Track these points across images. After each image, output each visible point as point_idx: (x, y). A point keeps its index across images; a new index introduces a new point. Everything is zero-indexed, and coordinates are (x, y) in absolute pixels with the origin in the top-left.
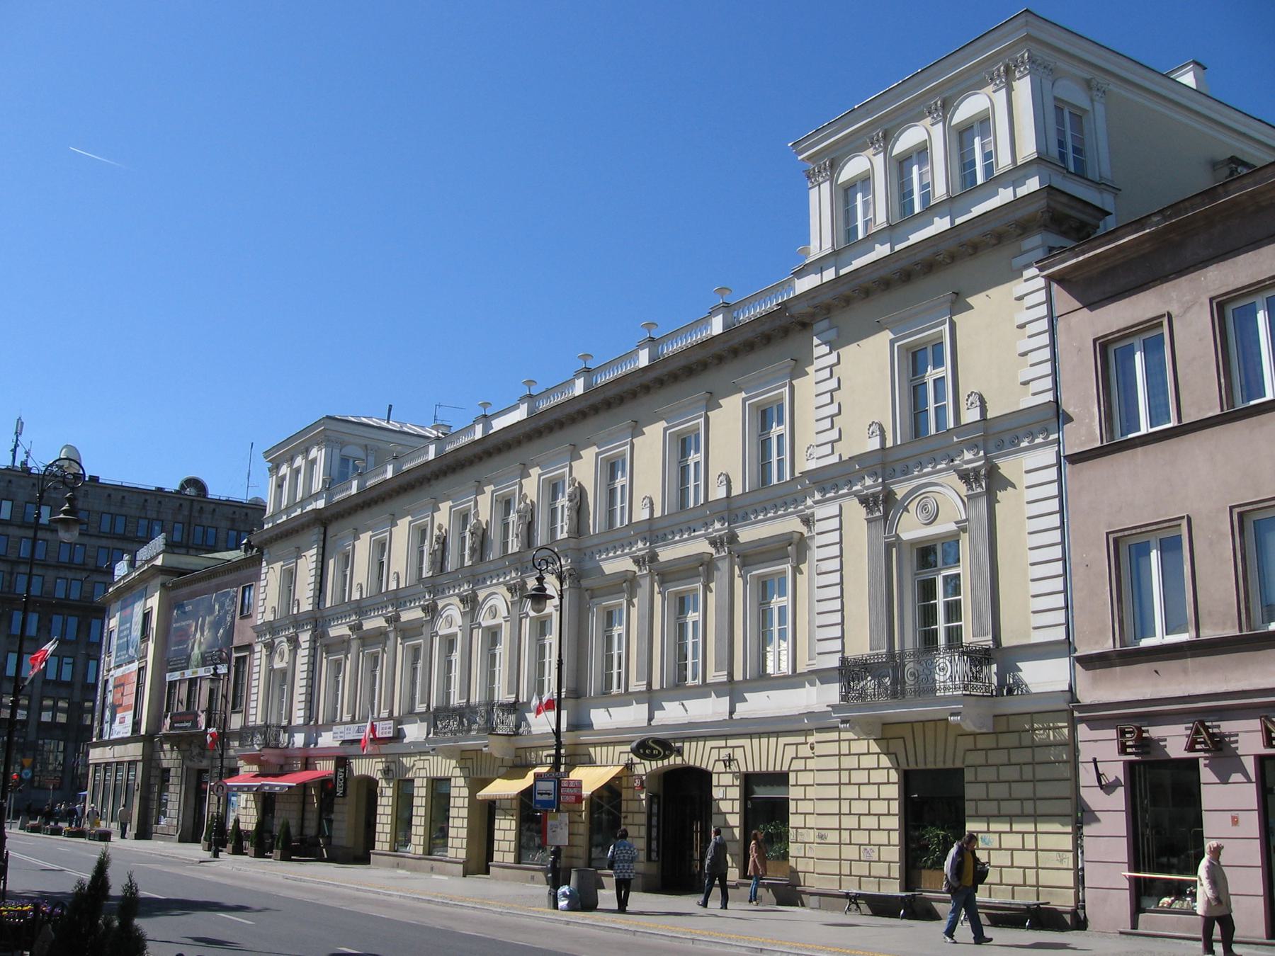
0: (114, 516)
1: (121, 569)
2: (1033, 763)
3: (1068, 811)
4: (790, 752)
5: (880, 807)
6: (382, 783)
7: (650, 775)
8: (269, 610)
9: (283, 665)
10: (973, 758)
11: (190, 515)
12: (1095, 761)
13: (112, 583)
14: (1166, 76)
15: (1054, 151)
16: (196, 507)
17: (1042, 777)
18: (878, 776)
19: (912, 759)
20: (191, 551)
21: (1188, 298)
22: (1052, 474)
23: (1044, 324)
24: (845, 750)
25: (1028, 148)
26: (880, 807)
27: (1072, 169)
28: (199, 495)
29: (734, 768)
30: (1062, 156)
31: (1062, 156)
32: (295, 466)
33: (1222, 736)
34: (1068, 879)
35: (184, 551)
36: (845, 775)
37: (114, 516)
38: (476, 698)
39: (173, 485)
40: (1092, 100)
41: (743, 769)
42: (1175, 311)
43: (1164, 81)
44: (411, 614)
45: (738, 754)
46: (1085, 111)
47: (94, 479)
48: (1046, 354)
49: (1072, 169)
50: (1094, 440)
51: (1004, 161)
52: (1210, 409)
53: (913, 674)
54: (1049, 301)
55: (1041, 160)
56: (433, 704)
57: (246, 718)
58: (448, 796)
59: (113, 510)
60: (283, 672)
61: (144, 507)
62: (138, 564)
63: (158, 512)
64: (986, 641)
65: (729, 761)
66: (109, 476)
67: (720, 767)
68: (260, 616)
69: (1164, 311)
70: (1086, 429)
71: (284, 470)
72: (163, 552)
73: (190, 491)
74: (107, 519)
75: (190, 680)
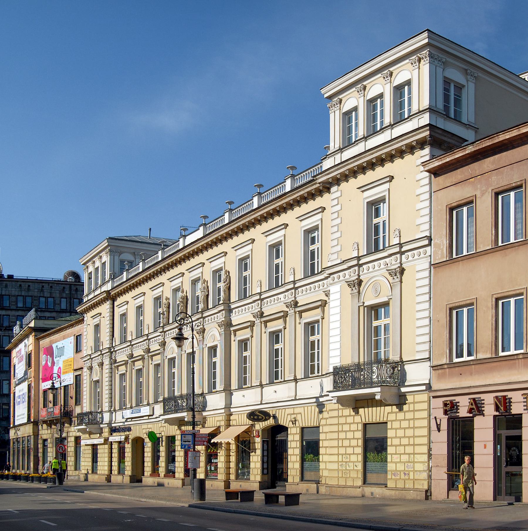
0: (25, 297)
1: (16, 329)
2: (414, 419)
6: (147, 440)
7: (263, 430)
8: (89, 349)
9: (97, 379)
11: (70, 293)
12: (435, 418)
13: (13, 337)
14: (518, 76)
15: (440, 106)
16: (74, 288)
17: (309, 479)
19: (367, 418)
20: (72, 314)
22: (426, 273)
23: (427, 196)
24: (340, 414)
25: (426, 103)
27: (452, 116)
28: (75, 282)
30: (447, 108)
31: (447, 108)
32: (89, 272)
34: (425, 475)
35: (68, 314)
36: (340, 426)
37: (25, 297)
38: (185, 392)
39: (59, 276)
40: (467, 81)
41: (301, 425)
43: (516, 78)
45: (299, 417)
46: (464, 86)
47: (11, 277)
48: (427, 211)
49: (452, 116)
50: (444, 257)
51: (415, 109)
53: (373, 373)
54: (430, 183)
55: (431, 110)
56: (166, 396)
59: (23, 294)
60: (98, 381)
61: (42, 291)
62: (24, 326)
63: (51, 293)
64: (397, 359)
65: (294, 422)
66: (19, 274)
67: (291, 425)
68: (85, 352)
70: (440, 250)
72: (34, 319)
73: (71, 279)
74: (20, 299)
75: (65, 386)
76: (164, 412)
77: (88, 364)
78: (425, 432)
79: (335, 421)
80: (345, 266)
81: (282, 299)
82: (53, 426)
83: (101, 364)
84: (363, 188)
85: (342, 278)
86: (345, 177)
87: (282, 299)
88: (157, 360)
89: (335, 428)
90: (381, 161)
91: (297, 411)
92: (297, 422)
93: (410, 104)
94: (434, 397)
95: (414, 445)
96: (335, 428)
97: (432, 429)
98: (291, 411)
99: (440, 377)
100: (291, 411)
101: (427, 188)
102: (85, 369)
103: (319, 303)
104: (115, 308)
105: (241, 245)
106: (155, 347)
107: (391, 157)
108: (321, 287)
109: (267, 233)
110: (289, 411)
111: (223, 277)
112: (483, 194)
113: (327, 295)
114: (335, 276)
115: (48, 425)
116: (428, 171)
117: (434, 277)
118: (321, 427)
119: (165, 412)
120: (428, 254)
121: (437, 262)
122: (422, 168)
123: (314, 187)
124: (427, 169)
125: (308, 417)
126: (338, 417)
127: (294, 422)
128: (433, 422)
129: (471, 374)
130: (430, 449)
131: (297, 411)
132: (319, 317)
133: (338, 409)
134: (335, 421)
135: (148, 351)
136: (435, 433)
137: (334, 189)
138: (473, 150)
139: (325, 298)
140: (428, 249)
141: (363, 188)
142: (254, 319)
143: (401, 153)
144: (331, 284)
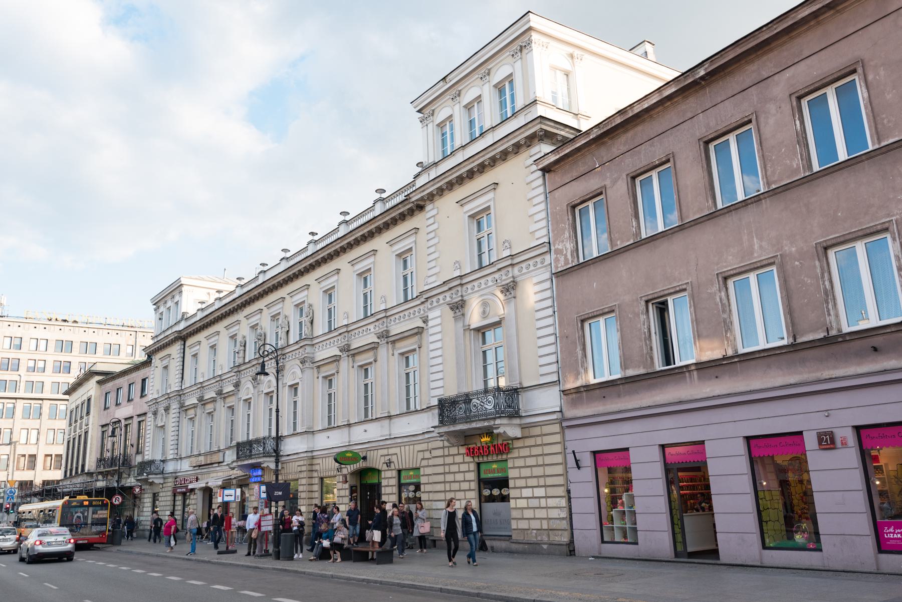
3: (562, 483)
4: (421, 455)
5: (465, 486)
10: (424, 463)
12: (574, 452)
18: (464, 467)
21: (616, 176)
24: (447, 453)
26: (465, 486)
29: (392, 467)
33: (101, 460)
42: (608, 183)
44: (228, 388)
45: (394, 458)
52: (628, 240)
54: (544, 184)
57: (143, 457)
58: (379, 485)
65: (389, 463)
69: (603, 184)
71: (162, 309)
76: (238, 458)
77: (153, 409)
78: (559, 470)
79: (440, 461)
80: (446, 288)
81: (372, 330)
82: (109, 477)
83: (167, 409)
84: (461, 203)
85: (442, 302)
86: (441, 191)
87: (372, 330)
88: (231, 401)
89: (440, 470)
90: (482, 168)
91: (391, 451)
92: (392, 465)
93: (513, 101)
94: (568, 427)
95: (545, 486)
96: (440, 470)
97: (568, 466)
98: (385, 452)
99: (574, 404)
100: (385, 452)
101: (541, 189)
102: (150, 415)
103: (416, 331)
104: (187, 349)
105: (326, 276)
106: (228, 388)
107: (494, 162)
108: (417, 314)
109: (352, 263)
110: (381, 452)
111: (305, 310)
112: (614, 182)
113: (424, 322)
114: (434, 299)
115: (103, 477)
116: (541, 170)
117: (557, 286)
118: (422, 469)
119: (238, 458)
120: (547, 262)
121: (560, 270)
122: (534, 167)
123: (408, 207)
124: (540, 166)
125: (405, 457)
126: (444, 473)
127: (389, 463)
128: (570, 458)
129: (619, 396)
130: (569, 492)
131: (391, 451)
132: (416, 346)
133: (443, 448)
134: (440, 461)
135: (220, 393)
136: (574, 474)
137: (429, 207)
138: (599, 133)
139: (422, 325)
140: (547, 257)
141: (461, 203)
142: (340, 354)
143: (505, 155)
144: (429, 309)
